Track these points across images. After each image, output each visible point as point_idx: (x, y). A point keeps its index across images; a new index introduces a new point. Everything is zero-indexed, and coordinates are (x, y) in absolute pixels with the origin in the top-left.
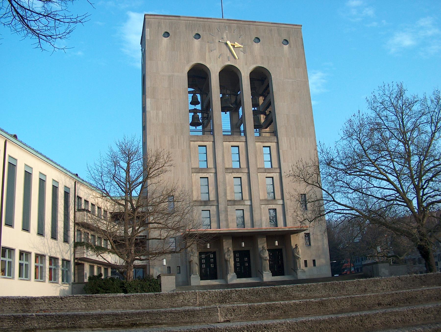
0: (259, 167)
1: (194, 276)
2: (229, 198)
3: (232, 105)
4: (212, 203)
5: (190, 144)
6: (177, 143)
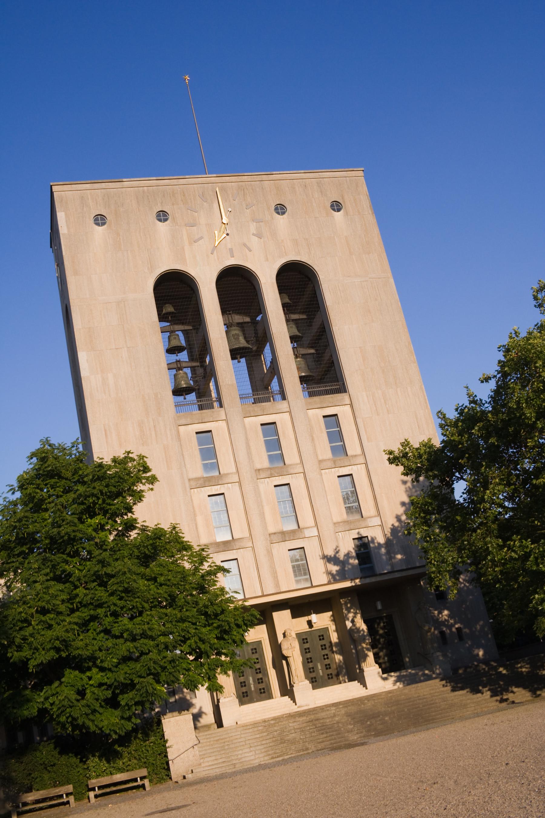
0: (320, 458)
1: (227, 700)
2: (272, 530)
3: (252, 346)
4: (238, 545)
5: (178, 432)
6: (153, 433)
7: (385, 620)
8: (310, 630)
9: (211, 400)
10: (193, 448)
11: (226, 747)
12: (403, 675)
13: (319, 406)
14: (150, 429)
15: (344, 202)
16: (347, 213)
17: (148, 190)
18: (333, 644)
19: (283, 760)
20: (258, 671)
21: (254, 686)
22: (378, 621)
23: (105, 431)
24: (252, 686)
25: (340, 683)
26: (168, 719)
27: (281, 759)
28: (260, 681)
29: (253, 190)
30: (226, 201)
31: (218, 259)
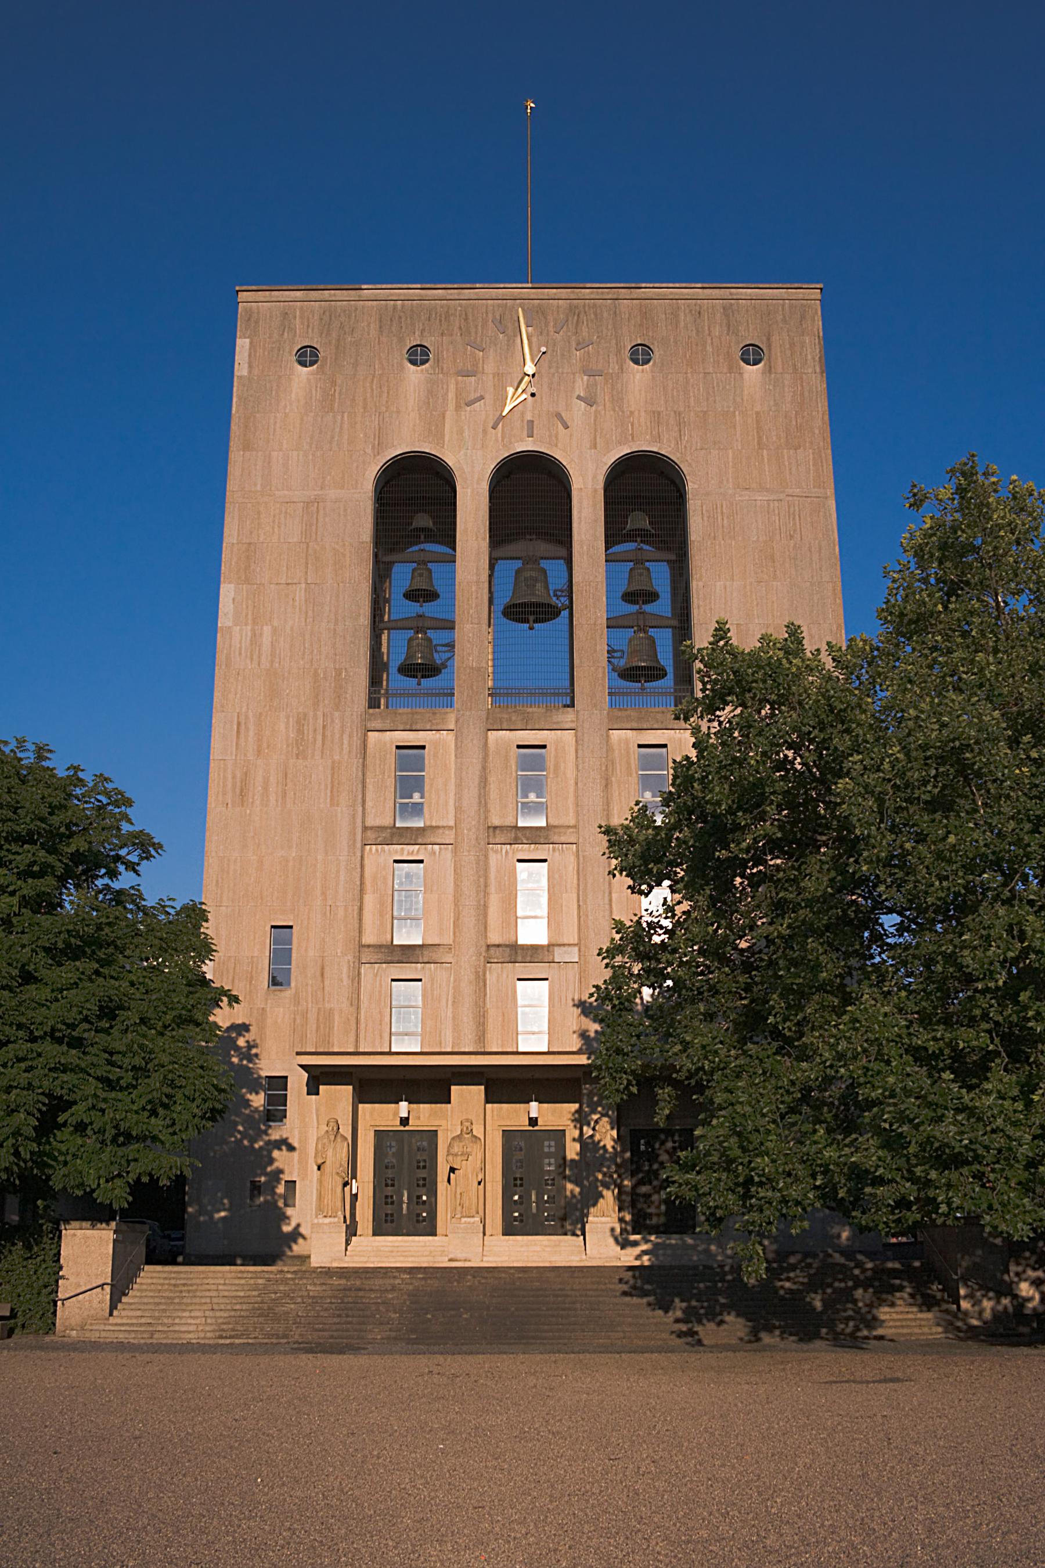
4: (427, 955)
6: (319, 738)
7: (676, 1138)
8: (531, 1128)
9: (379, 693)
10: (384, 774)
11: (177, 1301)
12: (670, 1245)
13: (635, 725)
14: (315, 730)
15: (769, 346)
16: (769, 369)
17: (403, 306)
18: (568, 1163)
19: (231, 1344)
20: (421, 1182)
21: (408, 1208)
22: (662, 1136)
23: (239, 724)
24: (405, 1206)
25: (566, 1234)
26: (72, 1232)
27: (228, 1341)
28: (388, 1200)
29: (596, 315)
30: (541, 333)
31: (503, 440)
